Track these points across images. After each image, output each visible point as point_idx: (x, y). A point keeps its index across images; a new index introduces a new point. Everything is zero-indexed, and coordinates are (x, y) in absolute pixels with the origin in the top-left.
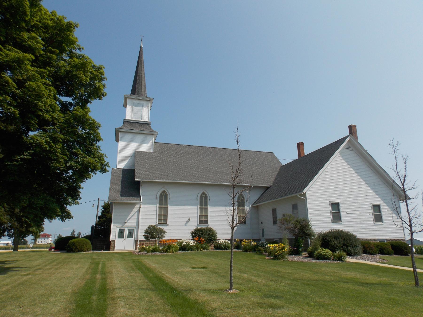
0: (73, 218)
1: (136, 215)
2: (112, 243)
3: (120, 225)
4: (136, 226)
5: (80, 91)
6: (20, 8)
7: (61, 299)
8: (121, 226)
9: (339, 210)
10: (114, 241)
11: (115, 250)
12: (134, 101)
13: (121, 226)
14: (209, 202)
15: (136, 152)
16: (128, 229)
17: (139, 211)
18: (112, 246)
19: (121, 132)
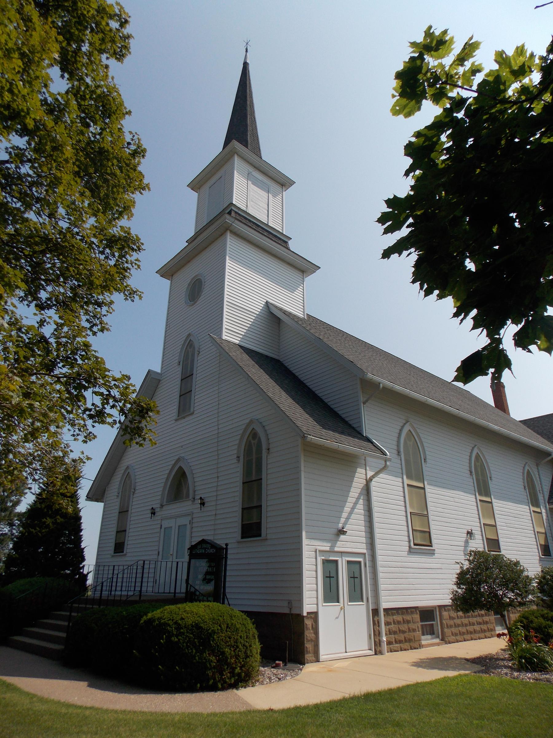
0: (399, 256)
1: (360, 508)
2: (308, 623)
3: (325, 544)
4: (364, 551)
5: (103, 294)
6: (8, 188)
7: (97, 279)
8: (328, 549)
9: (429, 529)
10: (314, 616)
11: (322, 657)
12: (251, 169)
13: (326, 546)
14: (492, 485)
15: (491, 70)
16: (349, 562)
17: (367, 490)
18: (308, 641)
19: (237, 235)
